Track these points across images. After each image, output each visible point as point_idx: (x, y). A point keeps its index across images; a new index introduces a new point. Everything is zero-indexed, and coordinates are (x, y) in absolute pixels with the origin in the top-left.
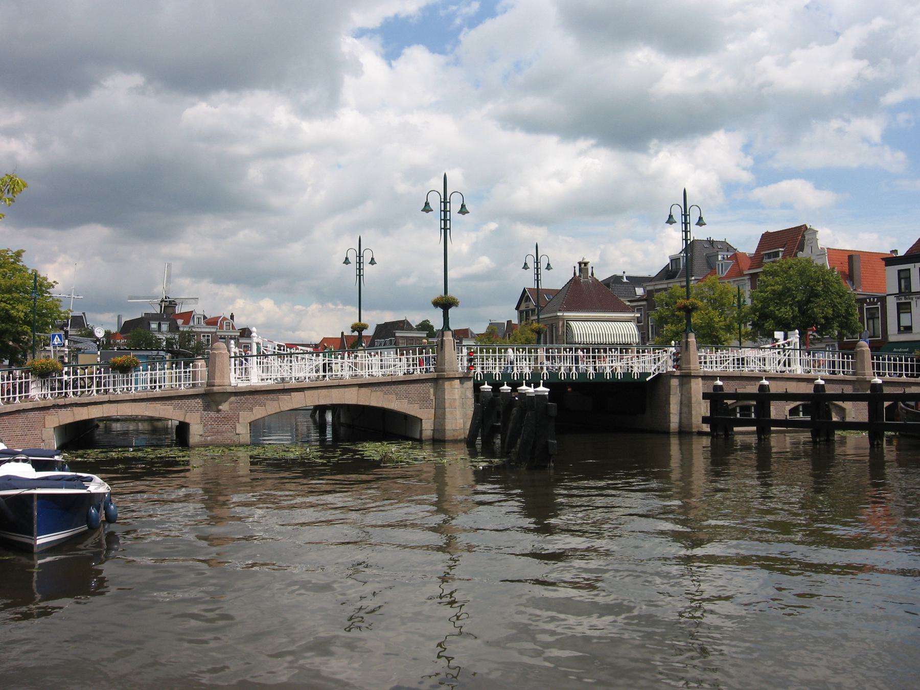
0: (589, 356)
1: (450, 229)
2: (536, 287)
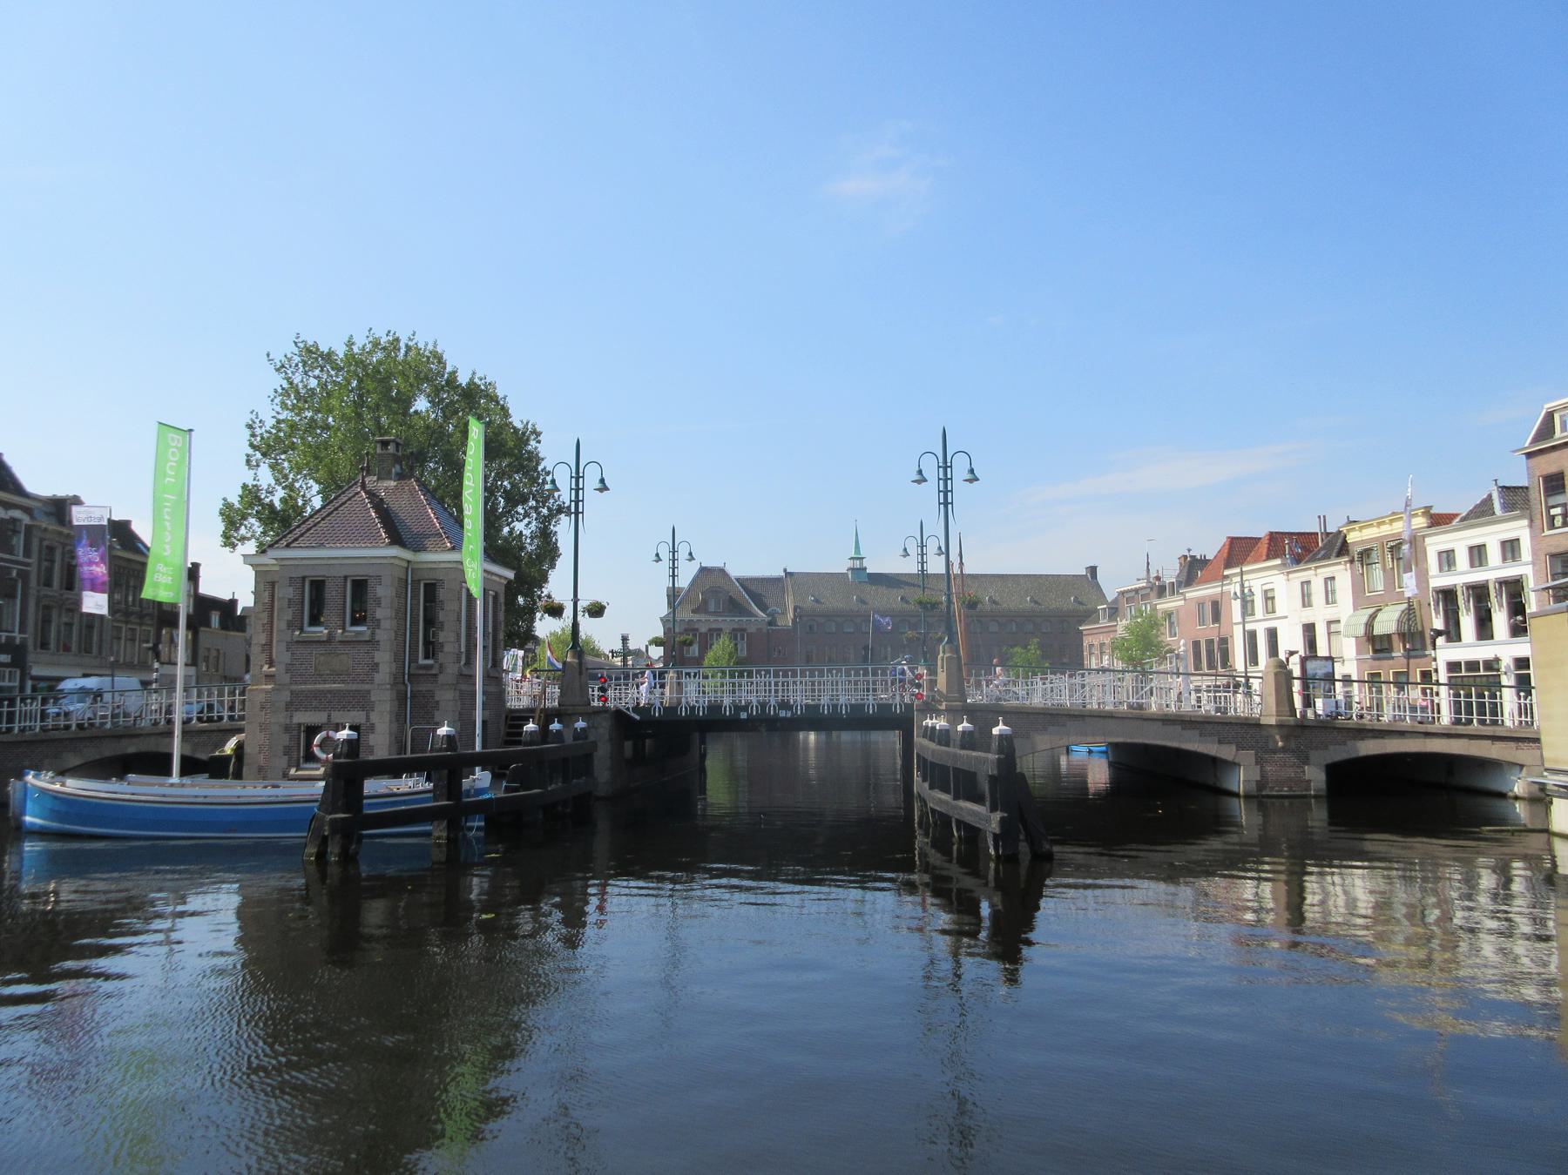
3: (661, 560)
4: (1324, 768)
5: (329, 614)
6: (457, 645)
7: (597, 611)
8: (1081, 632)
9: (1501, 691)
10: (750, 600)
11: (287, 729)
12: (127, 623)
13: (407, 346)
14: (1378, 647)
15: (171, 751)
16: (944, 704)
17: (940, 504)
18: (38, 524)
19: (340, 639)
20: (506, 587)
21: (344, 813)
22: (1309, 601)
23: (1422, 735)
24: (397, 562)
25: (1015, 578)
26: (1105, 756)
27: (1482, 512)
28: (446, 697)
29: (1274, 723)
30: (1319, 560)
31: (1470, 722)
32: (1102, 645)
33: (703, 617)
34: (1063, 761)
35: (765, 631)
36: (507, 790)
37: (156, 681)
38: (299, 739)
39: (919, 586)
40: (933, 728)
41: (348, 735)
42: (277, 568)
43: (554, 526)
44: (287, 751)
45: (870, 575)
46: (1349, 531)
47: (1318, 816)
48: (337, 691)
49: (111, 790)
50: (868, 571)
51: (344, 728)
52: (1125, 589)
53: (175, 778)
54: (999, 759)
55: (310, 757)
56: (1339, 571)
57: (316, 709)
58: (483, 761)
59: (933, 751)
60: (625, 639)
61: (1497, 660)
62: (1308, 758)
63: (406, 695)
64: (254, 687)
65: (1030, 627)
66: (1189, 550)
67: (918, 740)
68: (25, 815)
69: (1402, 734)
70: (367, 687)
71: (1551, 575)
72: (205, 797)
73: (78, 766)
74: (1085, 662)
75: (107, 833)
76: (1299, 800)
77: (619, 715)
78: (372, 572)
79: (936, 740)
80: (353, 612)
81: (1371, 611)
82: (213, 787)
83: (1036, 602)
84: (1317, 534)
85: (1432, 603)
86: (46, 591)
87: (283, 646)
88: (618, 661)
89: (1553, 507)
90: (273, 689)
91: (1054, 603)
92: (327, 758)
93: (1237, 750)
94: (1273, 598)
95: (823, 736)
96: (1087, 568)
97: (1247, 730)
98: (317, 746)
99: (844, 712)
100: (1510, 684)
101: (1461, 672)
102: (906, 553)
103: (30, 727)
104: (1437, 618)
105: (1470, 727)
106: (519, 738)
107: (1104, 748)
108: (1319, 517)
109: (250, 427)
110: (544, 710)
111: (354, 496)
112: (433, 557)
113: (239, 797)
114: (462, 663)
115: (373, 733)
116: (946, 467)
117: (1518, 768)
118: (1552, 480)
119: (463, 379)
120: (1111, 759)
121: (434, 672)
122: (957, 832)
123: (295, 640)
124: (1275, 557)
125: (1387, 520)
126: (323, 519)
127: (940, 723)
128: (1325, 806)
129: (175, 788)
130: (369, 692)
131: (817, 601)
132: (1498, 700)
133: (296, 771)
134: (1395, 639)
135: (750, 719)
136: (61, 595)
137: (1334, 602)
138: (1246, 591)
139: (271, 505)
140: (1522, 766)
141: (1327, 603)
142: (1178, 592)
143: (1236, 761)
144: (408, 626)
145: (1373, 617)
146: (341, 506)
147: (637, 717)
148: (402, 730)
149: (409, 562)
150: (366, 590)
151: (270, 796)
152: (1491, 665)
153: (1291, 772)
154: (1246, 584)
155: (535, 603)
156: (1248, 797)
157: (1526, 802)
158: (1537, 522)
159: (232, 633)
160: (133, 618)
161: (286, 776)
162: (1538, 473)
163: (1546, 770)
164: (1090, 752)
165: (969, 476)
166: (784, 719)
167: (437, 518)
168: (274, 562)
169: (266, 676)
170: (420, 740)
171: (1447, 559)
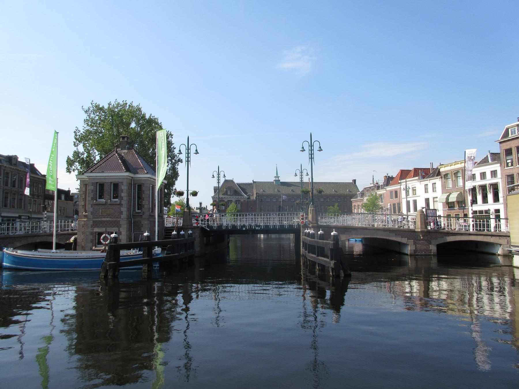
0: (261, 218)
1: (190, 161)
2: (218, 186)
3: (214, 177)
4: (436, 246)
5: (106, 195)
6: (149, 206)
7: (195, 194)
8: (352, 201)
9: (490, 220)
10: (241, 191)
11: (92, 233)
12: (38, 199)
13: (129, 105)
14: (450, 206)
15: (52, 241)
16: (311, 225)
17: (309, 158)
18: (3, 165)
19: (110, 203)
20: (164, 186)
21: (113, 262)
22: (427, 191)
23: (468, 235)
24: (128, 177)
25: (337, 183)
26: (361, 242)
27: (485, 162)
28: (145, 223)
29: (420, 231)
30: (431, 177)
31: (484, 230)
32: (358, 205)
33: (226, 197)
34: (347, 243)
35: (246, 201)
36: (167, 254)
37: (46, 217)
38: (96, 237)
39: (300, 187)
40: (309, 233)
41: (114, 235)
42: (88, 180)
43: (177, 166)
44: (92, 241)
45: (281, 183)
46: (440, 168)
47: (434, 262)
48: (109, 221)
49: (32, 254)
50: (280, 181)
51: (113, 233)
52: (367, 187)
53: (54, 250)
54: (334, 243)
55: (100, 243)
56: (437, 181)
57: (101, 227)
58: (158, 244)
59: (310, 240)
60: (201, 204)
61: (489, 210)
62: (431, 242)
63: (132, 222)
64: (80, 220)
65: (334, 200)
66: (387, 174)
67: (302, 237)
68: (3, 263)
69: (462, 234)
70: (119, 219)
71: (508, 182)
72: (65, 256)
73: (20, 246)
74: (353, 211)
75: (27, 268)
76: (428, 256)
77: (202, 229)
78: (120, 181)
79: (310, 237)
80: (114, 194)
81: (448, 194)
82: (67, 253)
83: (336, 192)
84: (430, 169)
85: (468, 191)
86: (6, 187)
87: (90, 206)
88: (198, 211)
89: (508, 160)
90: (87, 220)
91: (342, 192)
92: (105, 243)
93: (408, 240)
94: (415, 190)
95: (266, 236)
96: (352, 180)
97: (410, 234)
98: (102, 239)
99: (277, 228)
100: (493, 218)
101: (483, 214)
102: (296, 175)
103: (3, 233)
104: (469, 196)
105: (484, 232)
106: (171, 237)
107: (361, 239)
108: (431, 163)
109: (75, 132)
110: (178, 227)
111: (113, 155)
112: (143, 176)
113: (76, 256)
114: (150, 211)
115: (121, 235)
116: (311, 146)
117: (499, 246)
118: (508, 151)
119: (147, 117)
120: (363, 243)
121: (141, 214)
122: (318, 267)
123: (94, 203)
124: (416, 176)
125: (453, 164)
126: (103, 163)
127: (312, 231)
128: (436, 258)
129: (54, 253)
130: (119, 221)
131: (264, 191)
132: (489, 223)
133: (95, 248)
134: (456, 203)
135: (246, 230)
136: (11, 189)
137: (435, 191)
138: (408, 187)
139: (83, 158)
140: (501, 245)
141: (433, 191)
142: (384, 188)
143: (407, 243)
144: (132, 199)
145: (448, 196)
146: (109, 158)
147: (209, 230)
148: (131, 234)
149: (132, 177)
150: (118, 188)
151: (87, 256)
152: (487, 212)
153: (425, 247)
154: (408, 185)
155: (170, 191)
156: (411, 255)
157: (502, 256)
158: (503, 165)
159: (69, 202)
160: (36, 197)
161: (91, 249)
162: (503, 148)
163: (512, 246)
164: (356, 241)
165: (319, 149)
166: (258, 230)
167: (141, 163)
168: (87, 177)
169: (84, 216)
170: (136, 238)
171: (473, 177)
